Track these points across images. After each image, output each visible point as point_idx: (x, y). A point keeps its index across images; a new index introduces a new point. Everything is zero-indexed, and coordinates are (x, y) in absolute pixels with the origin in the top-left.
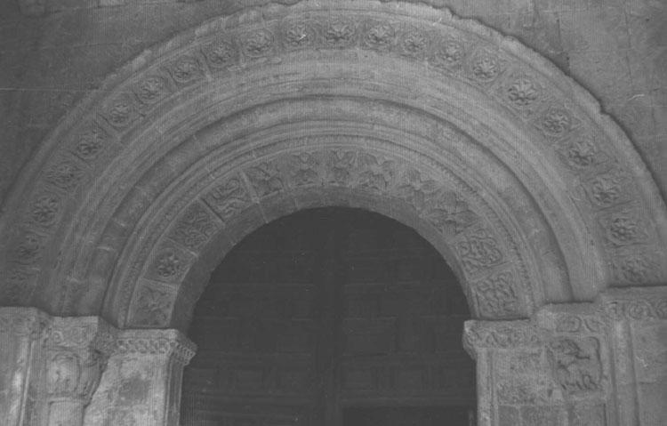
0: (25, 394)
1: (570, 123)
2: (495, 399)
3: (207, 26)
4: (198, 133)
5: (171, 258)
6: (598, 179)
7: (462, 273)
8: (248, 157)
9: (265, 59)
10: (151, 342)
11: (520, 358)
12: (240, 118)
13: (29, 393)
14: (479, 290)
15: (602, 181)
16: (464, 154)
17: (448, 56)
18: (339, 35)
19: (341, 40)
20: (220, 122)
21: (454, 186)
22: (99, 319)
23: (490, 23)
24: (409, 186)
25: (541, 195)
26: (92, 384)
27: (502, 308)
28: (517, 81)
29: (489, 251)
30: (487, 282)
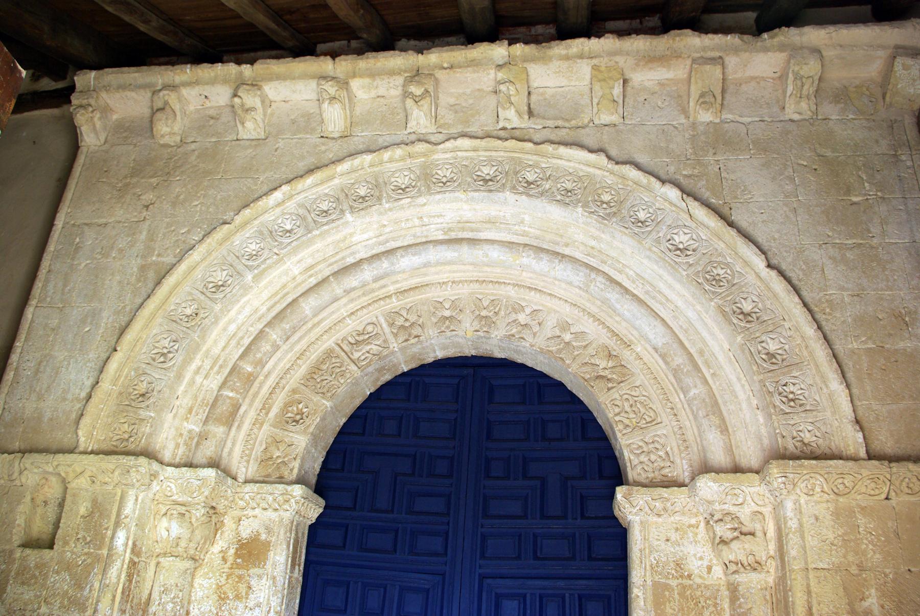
5: (300, 406)
11: (677, 529)
13: (133, 551)
16: (618, 306)
21: (605, 338)
22: (217, 473)
24: (559, 337)
26: (205, 543)
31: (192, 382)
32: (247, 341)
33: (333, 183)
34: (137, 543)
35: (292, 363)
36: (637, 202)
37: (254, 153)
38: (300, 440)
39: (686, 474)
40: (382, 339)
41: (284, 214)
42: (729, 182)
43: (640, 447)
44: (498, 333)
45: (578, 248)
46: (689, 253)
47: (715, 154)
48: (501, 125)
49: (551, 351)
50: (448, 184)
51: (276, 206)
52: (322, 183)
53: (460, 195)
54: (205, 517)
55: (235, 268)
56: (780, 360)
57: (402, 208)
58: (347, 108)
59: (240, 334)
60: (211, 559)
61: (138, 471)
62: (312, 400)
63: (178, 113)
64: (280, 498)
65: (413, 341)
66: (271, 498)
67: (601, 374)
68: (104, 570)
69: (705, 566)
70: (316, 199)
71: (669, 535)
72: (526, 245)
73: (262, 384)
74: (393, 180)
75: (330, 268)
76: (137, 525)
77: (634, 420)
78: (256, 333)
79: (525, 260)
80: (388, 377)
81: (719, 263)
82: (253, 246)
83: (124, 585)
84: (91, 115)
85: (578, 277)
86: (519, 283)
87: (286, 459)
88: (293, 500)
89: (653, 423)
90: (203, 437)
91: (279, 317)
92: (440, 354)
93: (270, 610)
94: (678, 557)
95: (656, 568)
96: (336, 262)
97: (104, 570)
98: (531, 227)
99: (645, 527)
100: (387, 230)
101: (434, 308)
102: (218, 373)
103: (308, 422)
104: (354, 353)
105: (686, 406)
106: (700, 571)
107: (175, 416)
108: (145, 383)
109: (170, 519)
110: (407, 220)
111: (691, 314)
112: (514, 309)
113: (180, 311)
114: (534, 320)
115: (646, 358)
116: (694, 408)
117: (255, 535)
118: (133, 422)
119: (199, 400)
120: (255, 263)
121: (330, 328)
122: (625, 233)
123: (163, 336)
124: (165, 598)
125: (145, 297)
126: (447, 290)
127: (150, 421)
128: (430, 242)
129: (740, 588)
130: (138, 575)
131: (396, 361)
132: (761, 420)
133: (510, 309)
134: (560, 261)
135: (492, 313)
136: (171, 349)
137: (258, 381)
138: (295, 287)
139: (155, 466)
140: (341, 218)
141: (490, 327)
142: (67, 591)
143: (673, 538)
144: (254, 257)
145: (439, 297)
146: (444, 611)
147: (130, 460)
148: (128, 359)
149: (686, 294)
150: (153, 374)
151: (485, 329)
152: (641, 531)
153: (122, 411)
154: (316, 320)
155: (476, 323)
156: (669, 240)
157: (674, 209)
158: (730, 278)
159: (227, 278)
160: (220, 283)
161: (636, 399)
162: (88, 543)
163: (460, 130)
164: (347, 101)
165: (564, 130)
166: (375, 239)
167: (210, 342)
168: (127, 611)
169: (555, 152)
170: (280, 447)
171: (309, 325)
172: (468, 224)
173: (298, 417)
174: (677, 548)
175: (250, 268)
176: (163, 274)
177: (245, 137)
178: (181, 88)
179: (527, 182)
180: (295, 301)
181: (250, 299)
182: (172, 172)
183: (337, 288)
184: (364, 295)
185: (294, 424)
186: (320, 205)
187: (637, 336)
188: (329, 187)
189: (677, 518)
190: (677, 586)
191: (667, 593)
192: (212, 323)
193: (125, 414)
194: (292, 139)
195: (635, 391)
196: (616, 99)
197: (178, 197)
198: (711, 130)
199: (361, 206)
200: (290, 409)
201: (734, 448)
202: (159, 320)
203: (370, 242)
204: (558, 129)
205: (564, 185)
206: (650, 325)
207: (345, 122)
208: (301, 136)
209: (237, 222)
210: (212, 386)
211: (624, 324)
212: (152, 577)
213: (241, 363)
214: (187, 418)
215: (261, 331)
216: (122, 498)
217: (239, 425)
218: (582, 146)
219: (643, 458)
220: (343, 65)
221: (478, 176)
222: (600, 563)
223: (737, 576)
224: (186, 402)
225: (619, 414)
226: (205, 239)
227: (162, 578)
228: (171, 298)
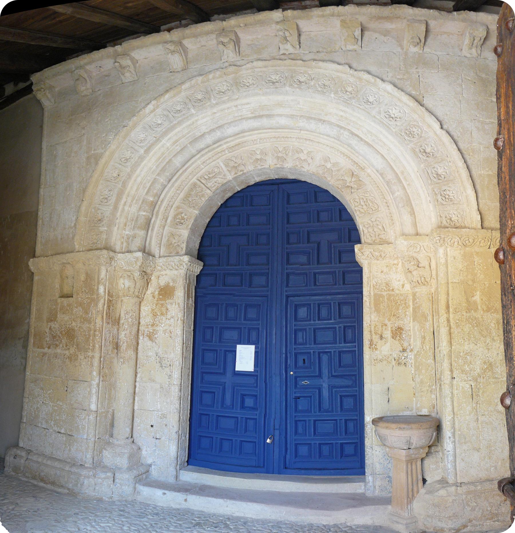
0: (106, 296)
1: (422, 133)
2: (372, 289)
3: (189, 83)
4: (191, 143)
5: (183, 215)
6: (436, 166)
7: (355, 216)
8: (223, 153)
9: (227, 97)
10: (175, 264)
11: (387, 266)
12: (215, 131)
13: (109, 295)
14: (364, 226)
15: (438, 167)
16: (356, 148)
17: (347, 91)
18: (275, 81)
19: (277, 84)
20: (203, 135)
22: (143, 254)
23: (376, 74)
24: (323, 165)
25: (402, 173)
26: (143, 289)
27: (377, 237)
28: (390, 108)
29: (371, 204)
30: (369, 222)
31: (123, 209)
32: (148, 185)
38: (185, 233)
50: (251, 86)
56: (443, 178)
58: (183, 55)
60: (147, 297)
63: (87, 79)
71: (383, 269)
80: (229, 195)
82: (142, 136)
83: (106, 311)
84: (44, 92)
92: (258, 179)
99: (370, 266)
105: (394, 201)
107: (118, 228)
109: (124, 279)
112: (297, 151)
124: (127, 316)
129: (417, 294)
131: (232, 185)
132: (432, 209)
139: (112, 254)
141: (283, 161)
142: (82, 316)
143: (385, 271)
150: (103, 209)
152: (368, 268)
162: (87, 293)
164: (182, 51)
168: (110, 323)
174: (387, 276)
175: (141, 147)
177: (126, 81)
190: (386, 295)
195: (367, 194)
200: (178, 217)
208: (158, 74)
211: (361, 157)
216: (99, 270)
217: (152, 229)
220: (176, 34)
227: (124, 307)
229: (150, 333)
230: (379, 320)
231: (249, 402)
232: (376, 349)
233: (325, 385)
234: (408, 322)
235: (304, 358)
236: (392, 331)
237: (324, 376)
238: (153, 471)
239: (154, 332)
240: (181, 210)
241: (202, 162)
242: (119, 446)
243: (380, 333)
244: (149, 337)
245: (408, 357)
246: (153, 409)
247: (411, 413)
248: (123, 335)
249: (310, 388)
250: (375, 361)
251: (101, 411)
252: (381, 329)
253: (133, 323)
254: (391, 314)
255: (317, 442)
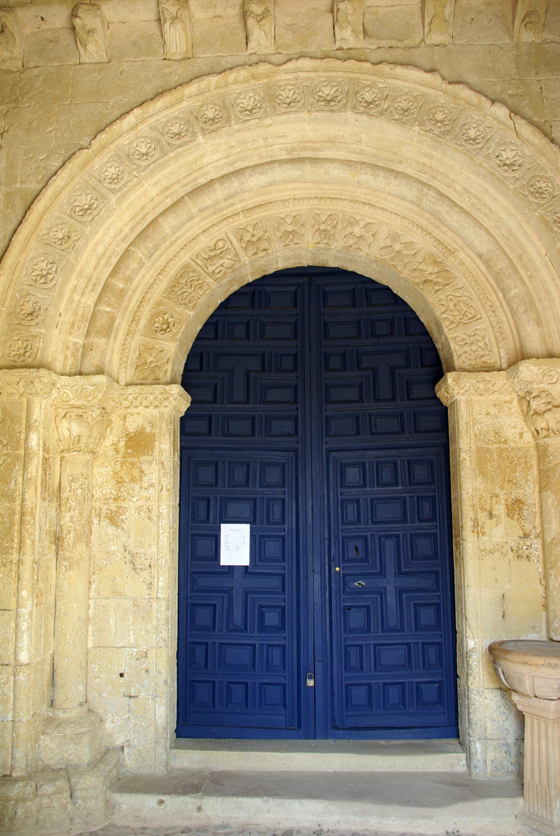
5: (166, 317)
11: (495, 405)
12: (231, 179)
16: (448, 218)
21: (430, 246)
22: (107, 378)
25: (520, 258)
26: (100, 439)
31: (71, 300)
32: (114, 260)
33: (182, 106)
34: (46, 443)
35: (154, 278)
36: (469, 120)
37: (100, 77)
39: (503, 360)
40: (233, 253)
41: (137, 138)
42: (550, 101)
43: (464, 339)
44: (337, 244)
45: (411, 165)
46: (515, 168)
47: (537, 74)
48: (338, 45)
49: (385, 260)
51: (130, 130)
52: (172, 105)
53: (305, 115)
54: (100, 416)
55: (99, 192)
57: (249, 129)
59: (108, 254)
60: (105, 451)
61: (41, 381)
62: (175, 311)
64: (160, 397)
65: (261, 254)
66: (151, 397)
67: (428, 278)
68: (24, 467)
69: (518, 433)
70: (167, 122)
71: (489, 410)
72: (362, 163)
73: (130, 298)
74: (239, 101)
75: (184, 189)
76: (44, 427)
77: (458, 317)
78: (122, 252)
79: (363, 178)
80: (236, 288)
81: (542, 177)
82: (112, 170)
83: (42, 477)
85: (411, 192)
86: (354, 199)
87: (159, 363)
88: (171, 398)
89: (474, 319)
90: (86, 349)
91: (142, 236)
92: (281, 265)
93: (162, 488)
94: (496, 427)
95: (479, 437)
96: (189, 183)
97: (24, 467)
98: (367, 146)
100: (235, 151)
101: (278, 223)
102: (93, 290)
103: (175, 330)
104: (209, 267)
106: (514, 437)
108: (30, 303)
109: (70, 421)
110: (253, 141)
111: (512, 224)
113: (52, 235)
114: (369, 232)
115: (468, 263)
116: (514, 306)
117: (140, 429)
118: (26, 339)
119: (79, 316)
120: (117, 186)
121: (186, 245)
122: (458, 150)
123: (40, 259)
125: (16, 223)
126: (289, 207)
127: (42, 336)
128: (275, 161)
129: (550, 449)
130: (50, 469)
133: (346, 222)
134: (395, 177)
135: (331, 226)
136: (50, 271)
137: (127, 296)
138: (154, 208)
140: (195, 140)
144: (115, 181)
145: (281, 213)
146: (300, 479)
147: (33, 373)
148: (11, 282)
149: (508, 206)
150: (38, 295)
151: (325, 242)
152: (466, 408)
153: (14, 330)
154: (173, 238)
155: (316, 236)
156: (498, 156)
157: (502, 127)
158: (551, 190)
159: (92, 201)
160: (86, 207)
161: (459, 299)
163: (299, 51)
165: (397, 50)
166: (224, 160)
167: (82, 263)
169: (391, 72)
170: (152, 354)
171: (168, 243)
172: (310, 144)
173: (165, 326)
174: (496, 420)
175: (114, 191)
176: (30, 200)
177: (87, 61)
178: (17, 9)
179: (366, 102)
180: (154, 221)
181: (114, 221)
182: (20, 99)
183: (192, 207)
184: (214, 213)
185: (162, 332)
186: (172, 128)
187: (461, 245)
188: (178, 110)
189: (495, 396)
191: (488, 455)
192: (84, 245)
193: (17, 332)
194: (135, 62)
195: (458, 292)
196: (447, 18)
197: (30, 123)
198: (534, 50)
199: (212, 128)
200: (157, 319)
201: (547, 338)
202: (33, 244)
203: (219, 163)
204: (392, 49)
205: (400, 104)
206: (476, 234)
207: (186, 43)
209: (95, 146)
210: (89, 302)
211: (450, 234)
212: (59, 470)
213: (113, 281)
214: (71, 333)
215: (127, 251)
216: (29, 405)
218: (417, 67)
219: (466, 348)
221: (320, 96)
222: (424, 434)
223: (547, 440)
224: (67, 317)
225: (445, 312)
226: (66, 164)
228: (42, 222)
229: (112, 511)
230: (485, 489)
231: (272, 618)
232: (484, 534)
233: (390, 589)
234: (531, 491)
235: (357, 545)
236: (507, 505)
237: (388, 572)
238: (127, 759)
239: (121, 510)
240: (162, 308)
241: (201, 231)
242: (69, 722)
243: (488, 509)
244: (111, 520)
245: (533, 546)
246: (121, 644)
247: (538, 636)
248: (67, 519)
249: (367, 593)
250: (483, 553)
251: (35, 661)
252: (489, 502)
253: (85, 498)
254: (505, 478)
255: (379, 681)
